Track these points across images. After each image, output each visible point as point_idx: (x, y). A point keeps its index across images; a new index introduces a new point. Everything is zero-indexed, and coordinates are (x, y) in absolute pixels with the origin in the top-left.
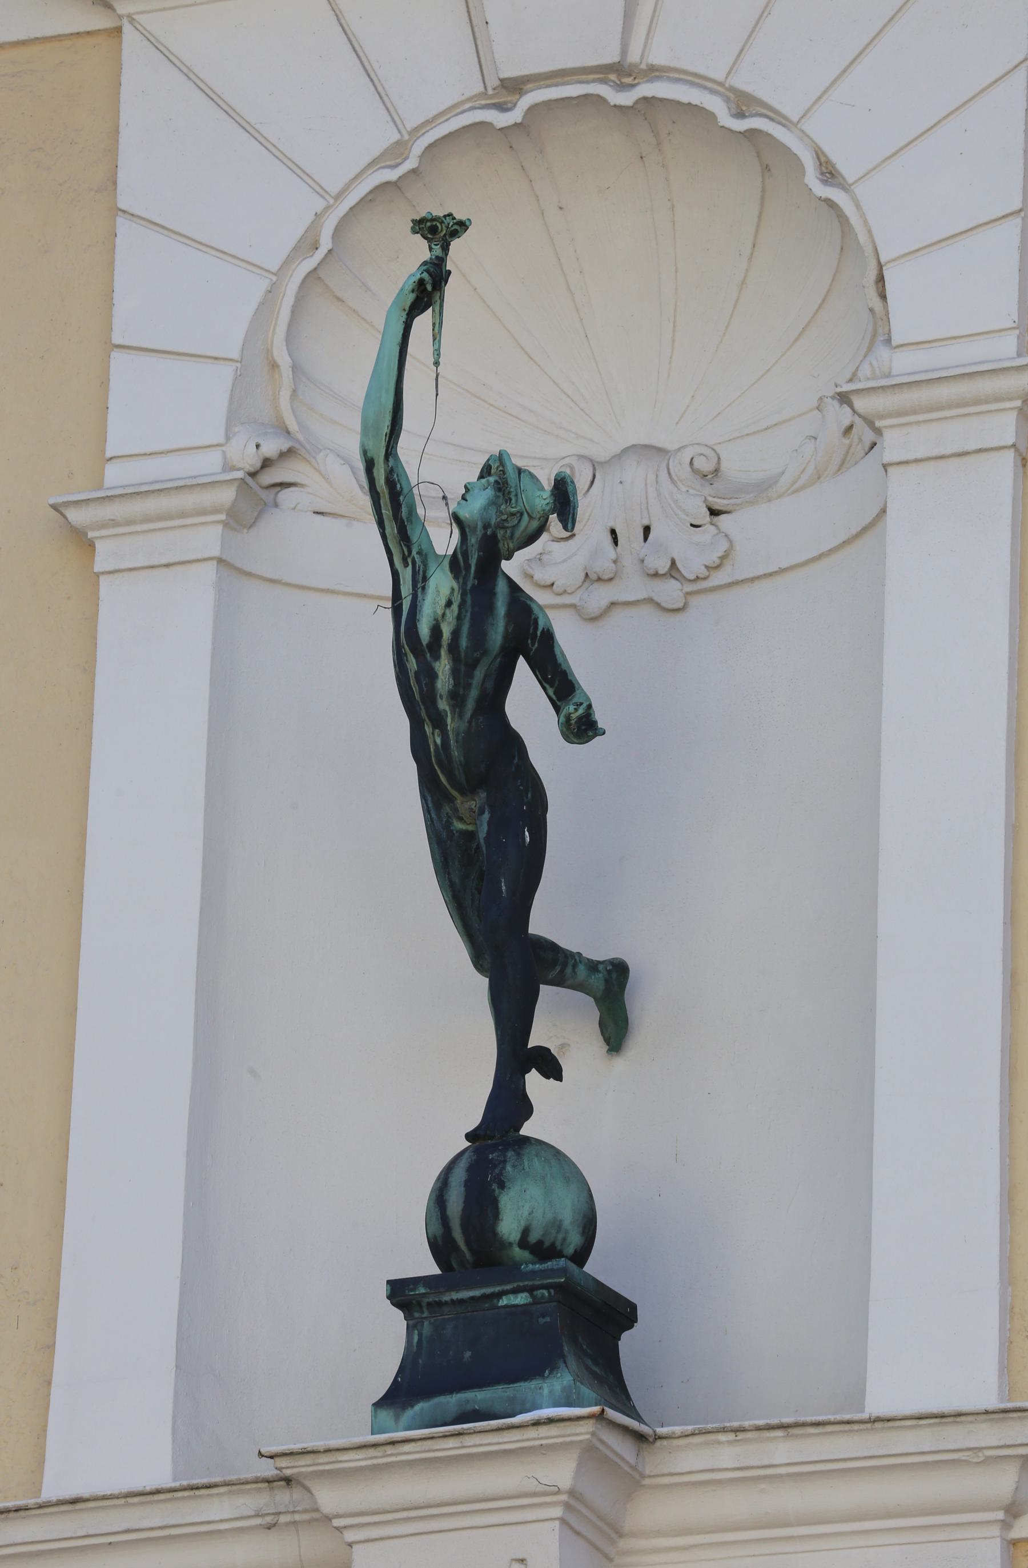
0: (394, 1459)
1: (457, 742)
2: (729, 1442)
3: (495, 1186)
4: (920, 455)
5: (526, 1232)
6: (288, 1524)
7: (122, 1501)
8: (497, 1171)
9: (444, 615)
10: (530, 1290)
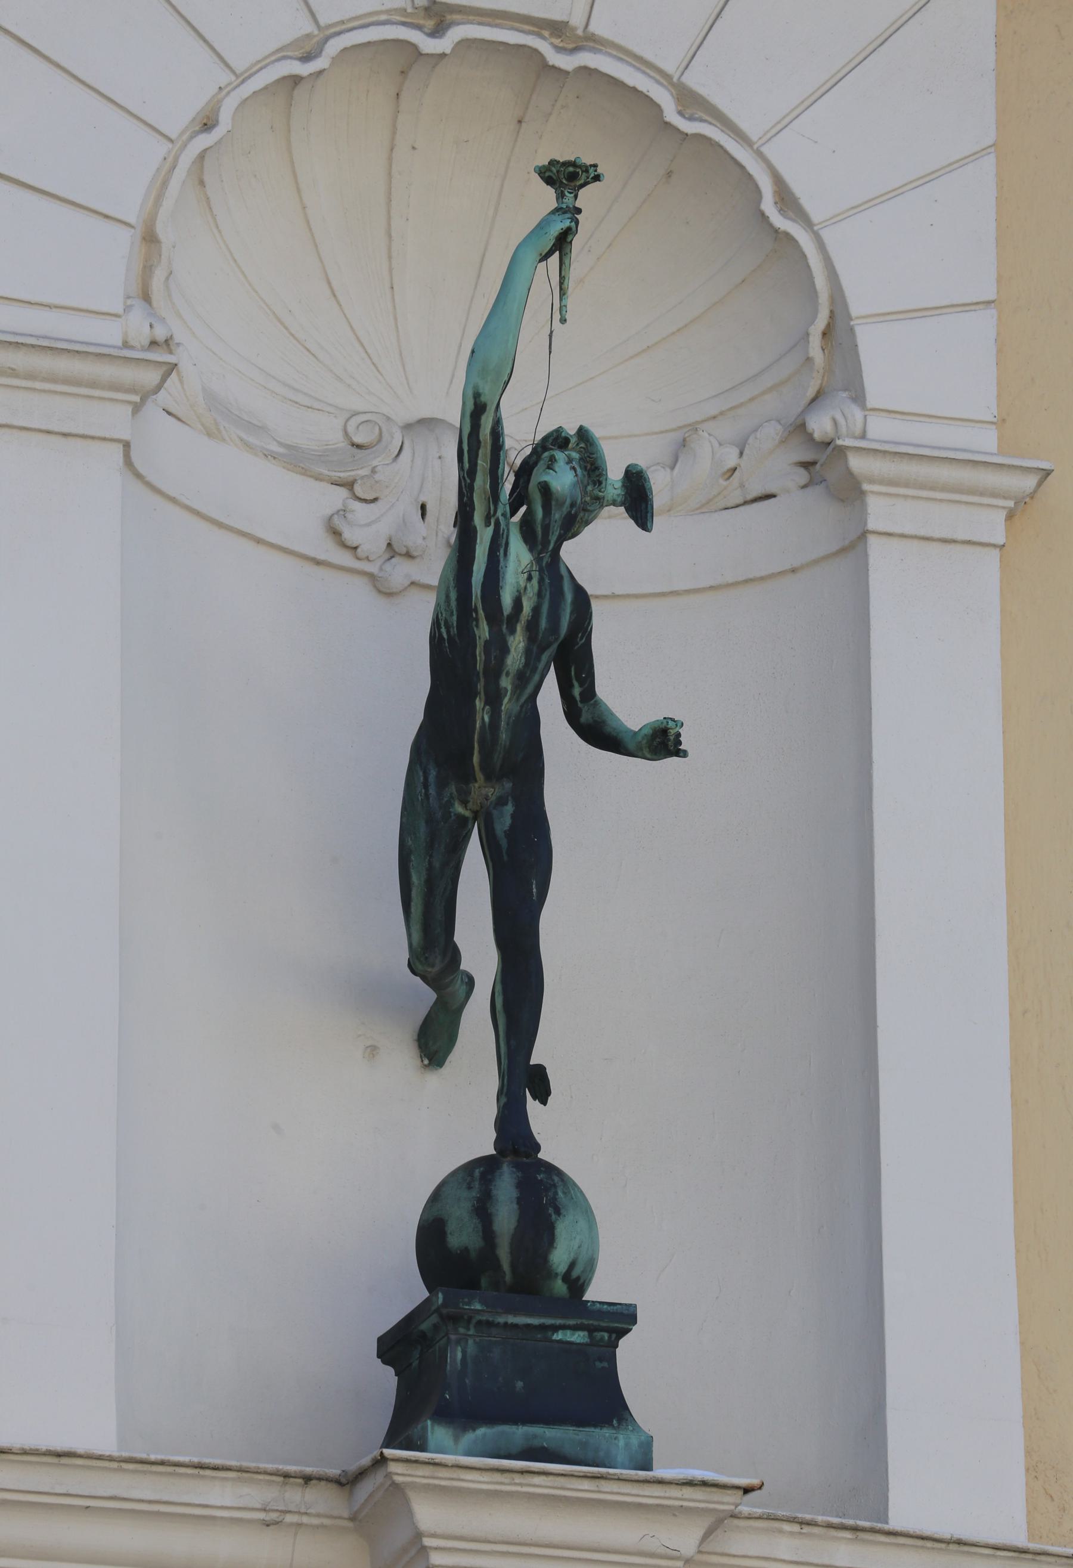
0: (519, 1488)
1: (508, 724)
2: (792, 1533)
3: (551, 1210)
4: (908, 530)
5: (572, 1265)
6: (291, 1524)
7: (115, 1465)
8: (551, 1194)
9: (526, 588)
10: (591, 1330)
